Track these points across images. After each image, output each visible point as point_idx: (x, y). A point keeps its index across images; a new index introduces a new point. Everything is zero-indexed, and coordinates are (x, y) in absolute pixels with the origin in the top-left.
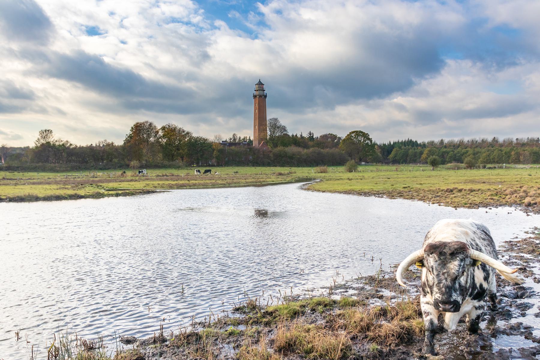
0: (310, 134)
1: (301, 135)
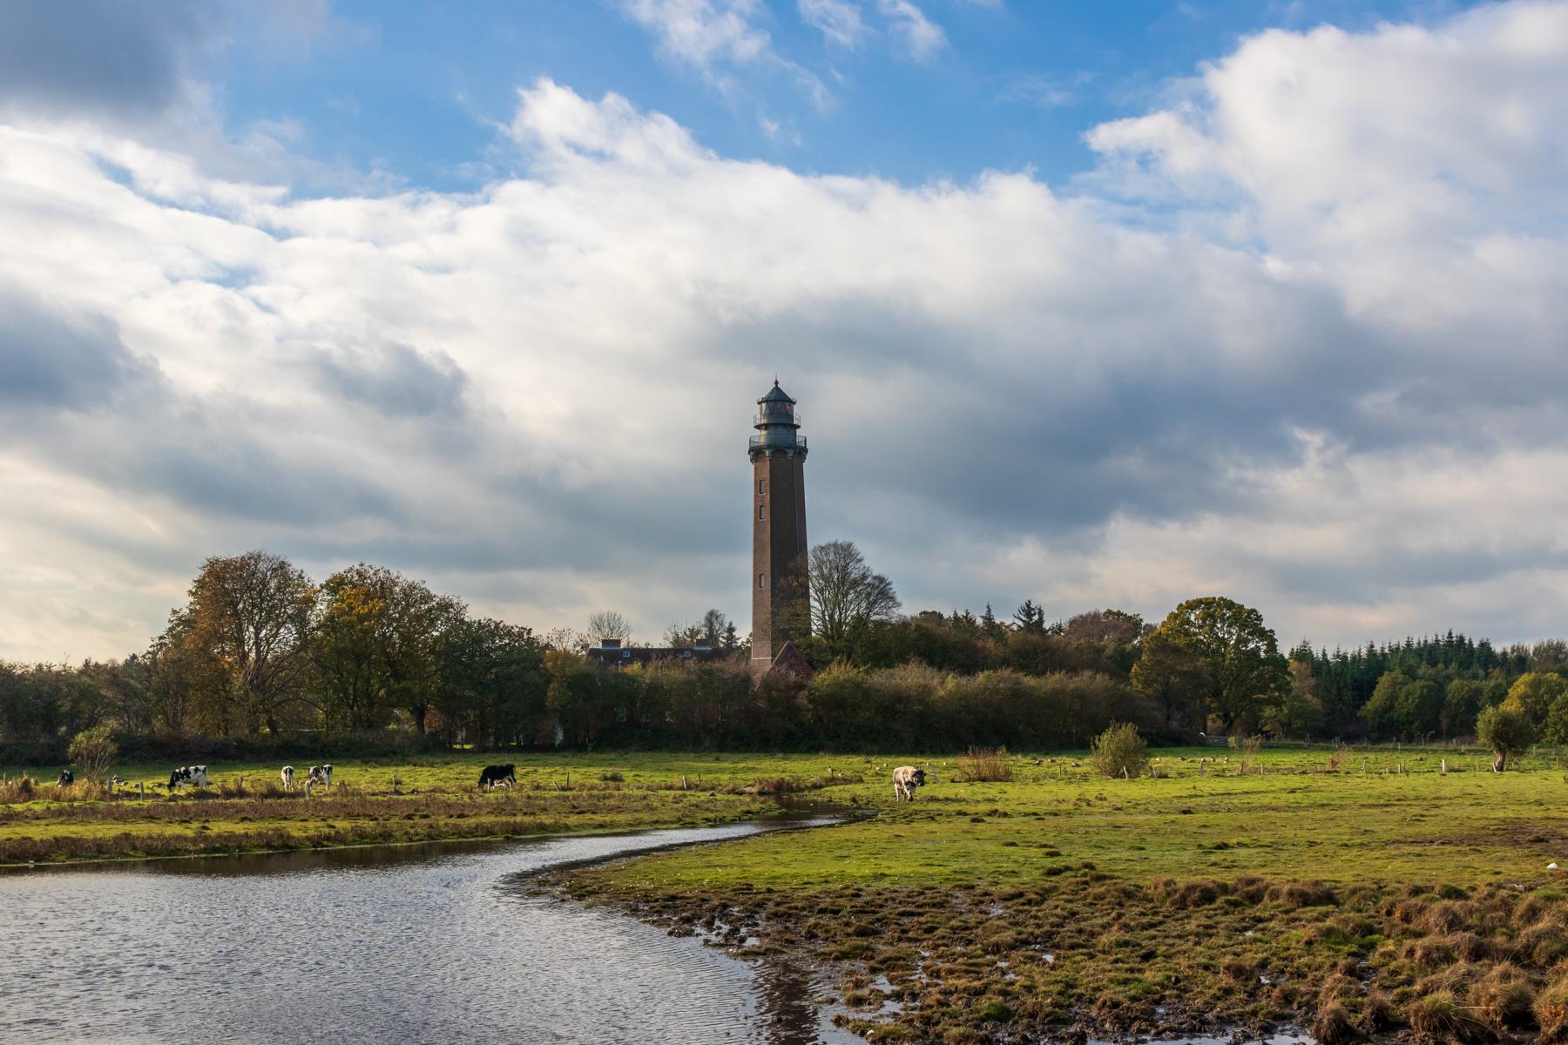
0: (1028, 610)
1: (988, 619)
